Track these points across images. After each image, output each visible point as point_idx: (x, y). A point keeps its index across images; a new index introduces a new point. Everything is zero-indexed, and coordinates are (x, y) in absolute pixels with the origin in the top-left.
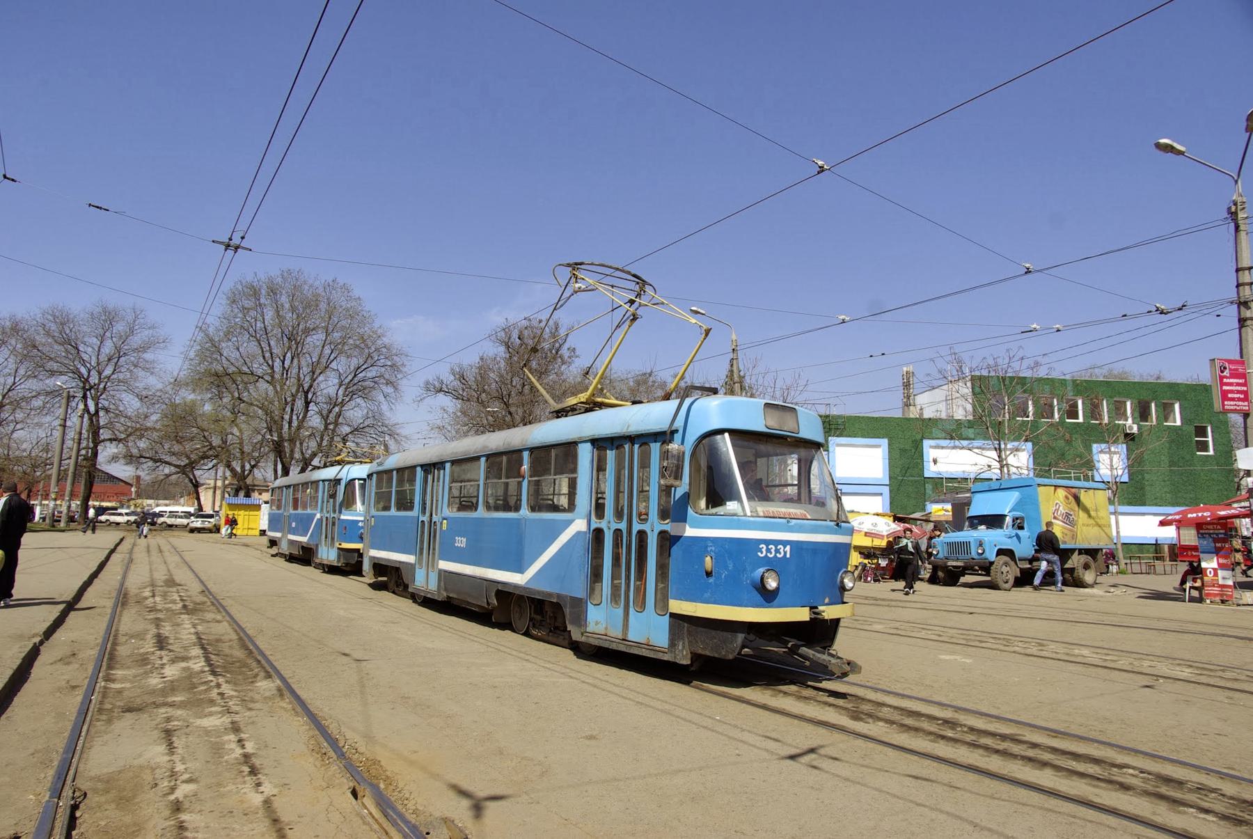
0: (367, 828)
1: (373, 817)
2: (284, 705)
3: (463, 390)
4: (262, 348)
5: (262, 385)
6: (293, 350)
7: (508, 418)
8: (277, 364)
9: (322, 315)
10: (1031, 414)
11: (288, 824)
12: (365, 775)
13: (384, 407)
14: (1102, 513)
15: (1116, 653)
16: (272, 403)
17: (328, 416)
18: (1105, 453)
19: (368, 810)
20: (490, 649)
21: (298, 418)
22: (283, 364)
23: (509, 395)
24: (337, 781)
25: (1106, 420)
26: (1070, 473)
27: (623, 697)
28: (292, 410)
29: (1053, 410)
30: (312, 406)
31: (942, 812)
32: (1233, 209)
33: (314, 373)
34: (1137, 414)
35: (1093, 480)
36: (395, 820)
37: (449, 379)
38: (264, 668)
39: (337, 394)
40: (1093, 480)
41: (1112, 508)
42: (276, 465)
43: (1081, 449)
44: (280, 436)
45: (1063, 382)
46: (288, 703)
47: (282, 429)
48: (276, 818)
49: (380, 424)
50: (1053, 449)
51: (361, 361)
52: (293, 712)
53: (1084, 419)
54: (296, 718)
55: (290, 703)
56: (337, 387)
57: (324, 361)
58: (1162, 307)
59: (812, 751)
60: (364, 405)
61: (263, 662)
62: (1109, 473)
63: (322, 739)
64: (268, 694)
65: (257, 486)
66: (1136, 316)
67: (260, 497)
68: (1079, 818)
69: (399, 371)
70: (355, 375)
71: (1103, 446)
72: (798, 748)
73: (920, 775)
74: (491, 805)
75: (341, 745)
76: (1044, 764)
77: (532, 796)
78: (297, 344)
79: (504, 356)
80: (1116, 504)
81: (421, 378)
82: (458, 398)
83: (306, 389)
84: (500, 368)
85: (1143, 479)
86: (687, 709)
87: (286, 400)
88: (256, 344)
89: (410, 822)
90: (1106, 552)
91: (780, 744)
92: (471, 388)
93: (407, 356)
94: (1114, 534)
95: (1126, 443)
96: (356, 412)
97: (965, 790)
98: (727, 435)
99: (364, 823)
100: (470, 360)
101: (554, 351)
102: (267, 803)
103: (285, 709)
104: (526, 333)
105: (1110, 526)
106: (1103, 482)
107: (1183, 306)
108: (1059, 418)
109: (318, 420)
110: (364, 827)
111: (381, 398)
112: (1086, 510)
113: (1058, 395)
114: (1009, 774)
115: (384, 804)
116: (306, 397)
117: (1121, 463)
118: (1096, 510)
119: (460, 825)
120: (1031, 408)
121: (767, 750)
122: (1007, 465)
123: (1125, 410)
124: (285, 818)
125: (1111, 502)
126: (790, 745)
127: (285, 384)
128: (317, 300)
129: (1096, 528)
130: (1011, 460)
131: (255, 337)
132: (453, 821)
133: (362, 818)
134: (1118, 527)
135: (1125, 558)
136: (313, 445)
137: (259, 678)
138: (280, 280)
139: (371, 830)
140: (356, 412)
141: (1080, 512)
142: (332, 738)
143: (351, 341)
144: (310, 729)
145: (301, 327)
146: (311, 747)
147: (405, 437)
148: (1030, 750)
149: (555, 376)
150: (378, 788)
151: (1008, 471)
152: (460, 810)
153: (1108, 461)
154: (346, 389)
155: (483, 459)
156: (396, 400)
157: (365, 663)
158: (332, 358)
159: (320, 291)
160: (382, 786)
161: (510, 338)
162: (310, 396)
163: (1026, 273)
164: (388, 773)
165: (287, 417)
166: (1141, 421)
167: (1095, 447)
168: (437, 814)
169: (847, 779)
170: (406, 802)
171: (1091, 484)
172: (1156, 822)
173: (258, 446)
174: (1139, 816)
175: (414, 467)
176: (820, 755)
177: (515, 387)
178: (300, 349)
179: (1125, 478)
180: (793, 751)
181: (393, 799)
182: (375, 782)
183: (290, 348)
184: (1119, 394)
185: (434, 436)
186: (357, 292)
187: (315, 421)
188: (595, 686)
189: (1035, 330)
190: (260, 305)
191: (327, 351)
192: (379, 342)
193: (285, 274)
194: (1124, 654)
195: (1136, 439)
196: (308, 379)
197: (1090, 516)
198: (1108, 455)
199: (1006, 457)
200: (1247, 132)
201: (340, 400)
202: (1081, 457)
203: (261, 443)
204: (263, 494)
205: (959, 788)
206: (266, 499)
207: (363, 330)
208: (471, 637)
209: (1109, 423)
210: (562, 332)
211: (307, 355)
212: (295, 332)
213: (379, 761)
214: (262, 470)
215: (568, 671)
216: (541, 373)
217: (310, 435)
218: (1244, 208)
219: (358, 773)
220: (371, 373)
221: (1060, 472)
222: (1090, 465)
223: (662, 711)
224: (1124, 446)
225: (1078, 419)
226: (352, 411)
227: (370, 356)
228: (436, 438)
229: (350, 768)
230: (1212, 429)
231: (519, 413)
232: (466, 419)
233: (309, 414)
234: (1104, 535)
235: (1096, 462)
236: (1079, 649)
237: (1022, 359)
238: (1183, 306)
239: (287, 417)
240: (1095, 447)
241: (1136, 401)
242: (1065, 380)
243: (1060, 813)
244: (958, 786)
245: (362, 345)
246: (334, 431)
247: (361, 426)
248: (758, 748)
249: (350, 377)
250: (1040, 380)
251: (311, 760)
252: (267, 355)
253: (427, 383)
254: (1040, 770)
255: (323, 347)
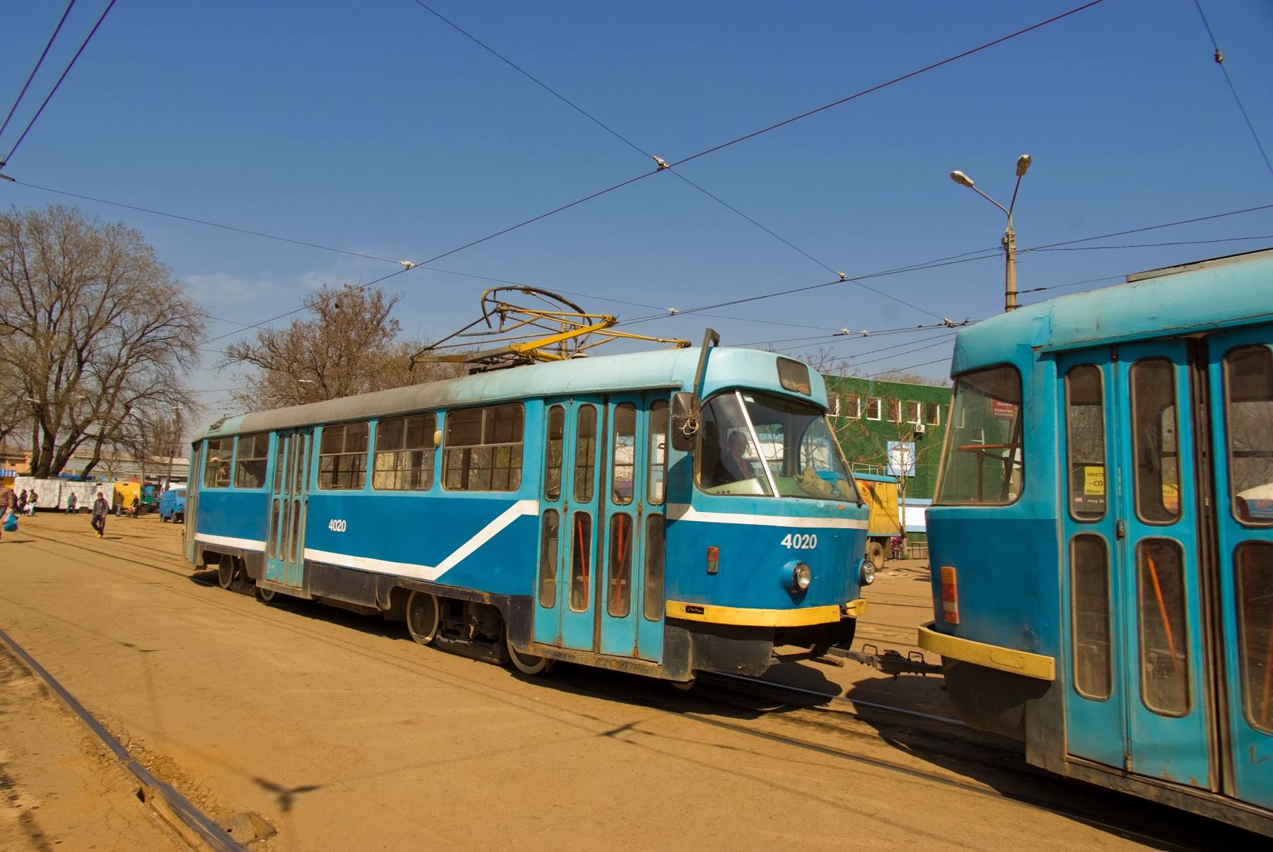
0: (157, 831)
1: (164, 819)
2: (49, 705)
3: (273, 358)
4: (20, 295)
5: (19, 338)
6: (64, 301)
7: (321, 391)
8: (42, 316)
9: (104, 263)
10: (837, 412)
11: (55, 837)
12: (155, 775)
13: (178, 372)
14: (892, 505)
15: (895, 629)
16: (33, 359)
17: (107, 379)
18: (898, 450)
19: (158, 812)
20: (298, 635)
21: (68, 378)
22: (50, 314)
23: (324, 367)
24: (119, 784)
25: (900, 420)
26: (868, 467)
27: (440, 681)
28: (61, 369)
29: (857, 408)
30: (86, 366)
31: (744, 775)
32: (1006, 241)
33: (90, 328)
34: (925, 416)
35: (887, 475)
36: (191, 820)
37: (256, 345)
38: (20, 664)
39: (119, 354)
40: (887, 475)
41: (900, 501)
42: (36, 432)
43: (878, 445)
44: (43, 397)
45: (866, 383)
46: (54, 703)
47: (46, 390)
48: (39, 833)
49: (172, 390)
50: (854, 444)
51: (151, 319)
52: (60, 712)
53: (882, 418)
54: (64, 719)
55: (57, 702)
56: (120, 346)
57: (104, 315)
58: (950, 321)
59: (628, 727)
60: (153, 368)
61: (19, 658)
62: (900, 468)
63: (99, 740)
64: (26, 694)
65: (10, 455)
66: (929, 327)
67: (13, 468)
68: (857, 772)
69: (197, 332)
70: (143, 335)
71: (897, 443)
72: (614, 725)
73: (726, 744)
74: (301, 798)
75: (123, 745)
76: (832, 728)
77: (347, 784)
78: (69, 293)
79: (320, 323)
80: (904, 496)
81: (223, 345)
82: (266, 367)
83: (79, 346)
84: (315, 337)
85: (927, 473)
86: (506, 692)
87: (52, 357)
88: (12, 289)
89: (209, 820)
90: (894, 540)
91: (597, 721)
92: (281, 357)
93: (207, 317)
94: (901, 521)
95: (915, 441)
96: (143, 375)
97: (764, 755)
98: (738, 394)
99: (153, 826)
100: (282, 326)
101: (375, 323)
102: (26, 818)
103: (50, 710)
104: (345, 301)
105: (898, 516)
106: (894, 476)
107: (966, 322)
108: (861, 416)
109: (95, 383)
110: (154, 830)
111: (175, 361)
112: (879, 502)
113: (862, 395)
114: (803, 739)
115: (178, 804)
116: (80, 355)
117: (910, 459)
118: (888, 502)
119: (266, 819)
120: (838, 406)
121: (585, 728)
122: (813, 458)
123: (916, 411)
124: (49, 831)
125: (900, 495)
126: (606, 722)
127: (52, 338)
128: (96, 245)
129: (887, 518)
130: (816, 454)
131: (12, 281)
132: (259, 816)
133: (151, 821)
134: (904, 517)
135: (908, 545)
136: (87, 410)
137: (13, 677)
138: (47, 217)
139: (162, 833)
140: (143, 375)
141: (874, 503)
142: (112, 738)
143: (139, 296)
144: (83, 730)
145: (75, 273)
146: (85, 749)
147: (203, 406)
148: (821, 717)
149: (375, 348)
150: (171, 787)
151: (813, 465)
152: (267, 805)
153: (899, 458)
154: (131, 349)
155: (318, 432)
156: (193, 364)
157: (151, 654)
158: (114, 313)
159: (102, 235)
160: (175, 785)
161: (327, 306)
162: (85, 354)
163: (841, 281)
164: (182, 771)
165: (53, 377)
166: (928, 422)
167: (890, 444)
168: (241, 809)
169: (660, 752)
170: (203, 800)
171: (884, 478)
172: (915, 769)
173: (12, 409)
174: (902, 765)
175: (267, 432)
176: (635, 731)
177: (331, 358)
178: (72, 300)
179: (913, 474)
180: (610, 728)
181: (188, 798)
182: (167, 781)
183: (59, 297)
184: (912, 397)
185: (237, 406)
186: (148, 242)
187: (90, 383)
188: (412, 671)
189: (845, 333)
190: (19, 244)
191: (109, 304)
192: (174, 299)
193: (55, 211)
194: (902, 629)
195: (923, 438)
196: (82, 334)
197: (882, 507)
198: (900, 452)
199: (813, 451)
200: (1017, 175)
201: (123, 361)
202: (878, 454)
203: (17, 406)
204: (17, 465)
205: (758, 754)
206: (21, 471)
207: (154, 284)
208: (278, 624)
209: (903, 423)
210: (385, 303)
211: (82, 308)
212: (66, 280)
213: (171, 759)
214: (18, 438)
215: (384, 656)
216: (360, 345)
217: (83, 400)
218: (1013, 241)
219: (146, 773)
220: (164, 333)
221: (860, 466)
222: (885, 460)
223: (481, 694)
224: (914, 444)
225: (877, 417)
226: (138, 375)
227: (162, 314)
228: (239, 408)
229: (136, 769)
230: (985, 432)
231: (334, 386)
232: (273, 389)
233: (83, 375)
234: (892, 523)
235: (889, 458)
236: (866, 627)
237: (833, 359)
238: (966, 322)
239: (53, 377)
240: (890, 444)
241: (925, 404)
242: (868, 381)
243: (842, 768)
244: (758, 751)
245: (154, 302)
246: (114, 395)
247: (149, 392)
248: (577, 727)
249: (136, 337)
250: (847, 380)
251: (85, 763)
252: (28, 303)
253: (231, 348)
254: (829, 733)
255: (104, 299)
